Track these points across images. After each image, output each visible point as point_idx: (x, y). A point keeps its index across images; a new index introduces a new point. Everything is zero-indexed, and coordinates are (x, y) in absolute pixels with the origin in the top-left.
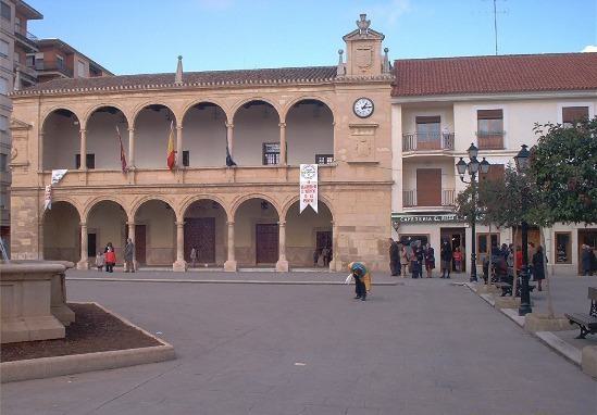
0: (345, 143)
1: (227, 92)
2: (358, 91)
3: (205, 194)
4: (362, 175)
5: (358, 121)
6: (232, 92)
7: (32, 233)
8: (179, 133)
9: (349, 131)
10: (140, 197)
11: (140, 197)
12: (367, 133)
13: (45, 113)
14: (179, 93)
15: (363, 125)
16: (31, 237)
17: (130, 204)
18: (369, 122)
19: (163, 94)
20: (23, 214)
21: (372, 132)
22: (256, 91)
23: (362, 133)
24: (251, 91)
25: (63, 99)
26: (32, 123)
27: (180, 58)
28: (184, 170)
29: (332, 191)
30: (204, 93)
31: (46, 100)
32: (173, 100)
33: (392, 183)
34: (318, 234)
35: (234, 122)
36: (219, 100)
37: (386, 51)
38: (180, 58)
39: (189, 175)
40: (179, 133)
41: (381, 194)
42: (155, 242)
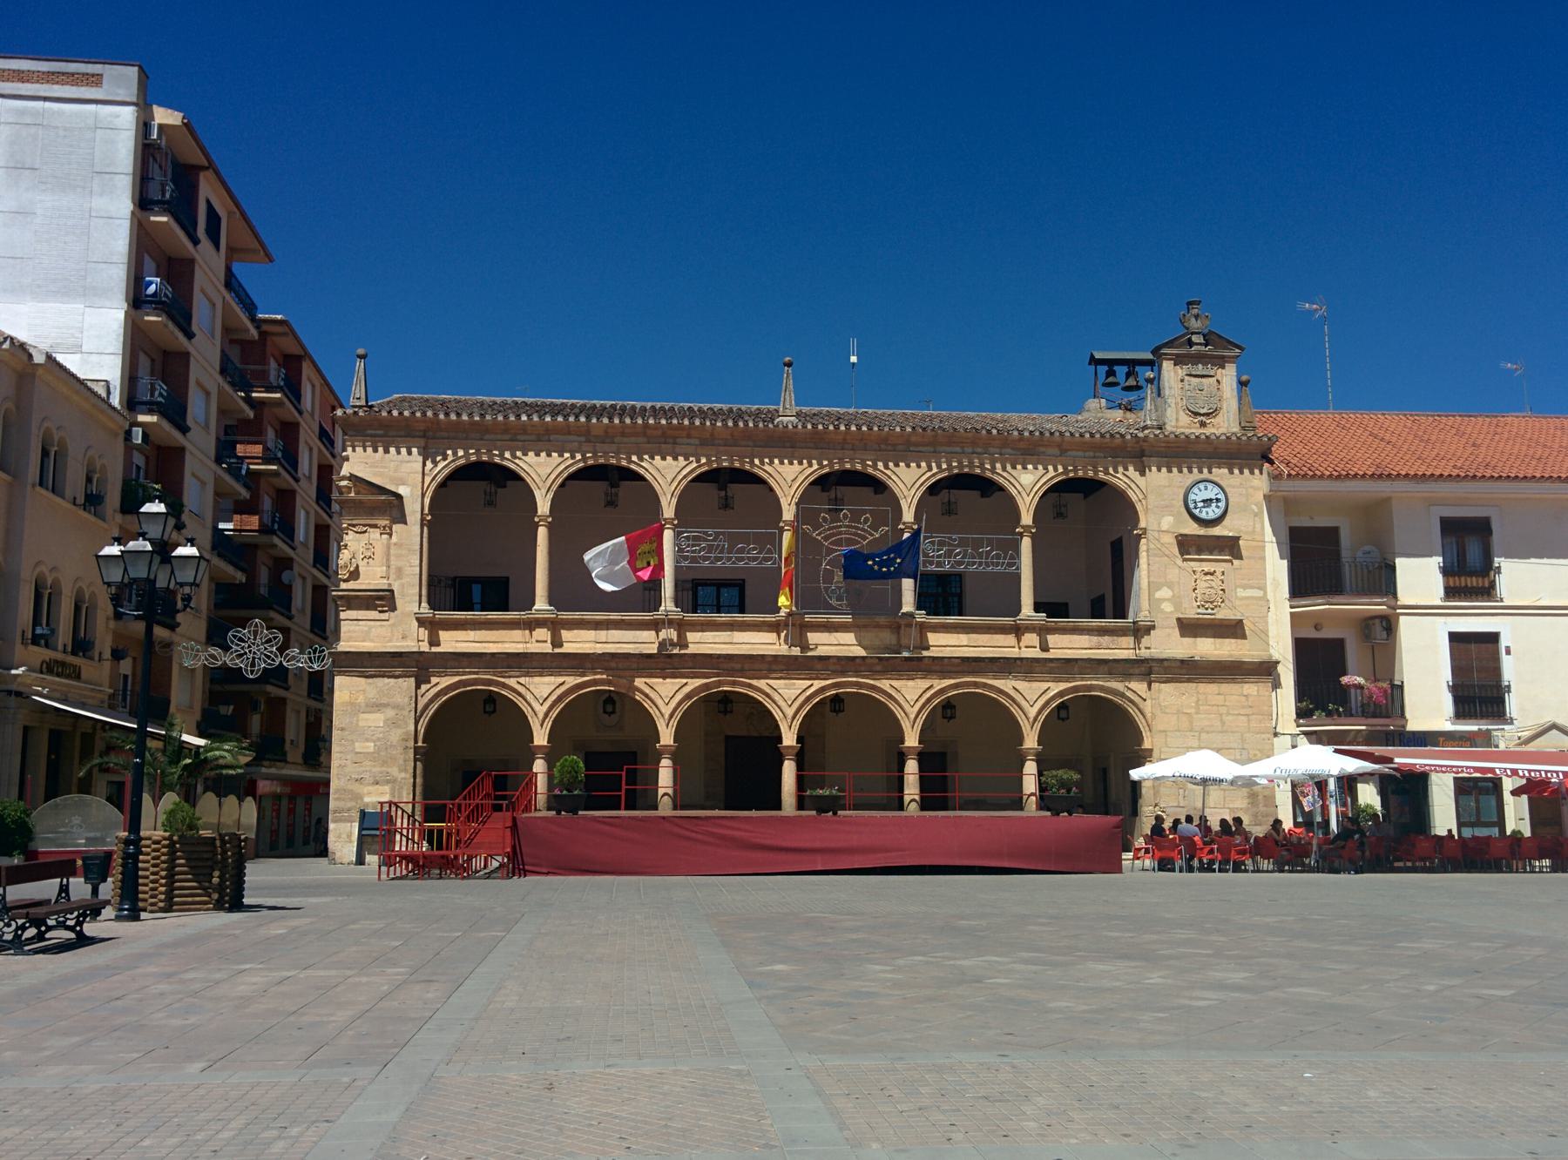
5: (1192, 529)
7: (394, 771)
15: (1208, 543)
16: (392, 781)
18: (1217, 531)
20: (376, 720)
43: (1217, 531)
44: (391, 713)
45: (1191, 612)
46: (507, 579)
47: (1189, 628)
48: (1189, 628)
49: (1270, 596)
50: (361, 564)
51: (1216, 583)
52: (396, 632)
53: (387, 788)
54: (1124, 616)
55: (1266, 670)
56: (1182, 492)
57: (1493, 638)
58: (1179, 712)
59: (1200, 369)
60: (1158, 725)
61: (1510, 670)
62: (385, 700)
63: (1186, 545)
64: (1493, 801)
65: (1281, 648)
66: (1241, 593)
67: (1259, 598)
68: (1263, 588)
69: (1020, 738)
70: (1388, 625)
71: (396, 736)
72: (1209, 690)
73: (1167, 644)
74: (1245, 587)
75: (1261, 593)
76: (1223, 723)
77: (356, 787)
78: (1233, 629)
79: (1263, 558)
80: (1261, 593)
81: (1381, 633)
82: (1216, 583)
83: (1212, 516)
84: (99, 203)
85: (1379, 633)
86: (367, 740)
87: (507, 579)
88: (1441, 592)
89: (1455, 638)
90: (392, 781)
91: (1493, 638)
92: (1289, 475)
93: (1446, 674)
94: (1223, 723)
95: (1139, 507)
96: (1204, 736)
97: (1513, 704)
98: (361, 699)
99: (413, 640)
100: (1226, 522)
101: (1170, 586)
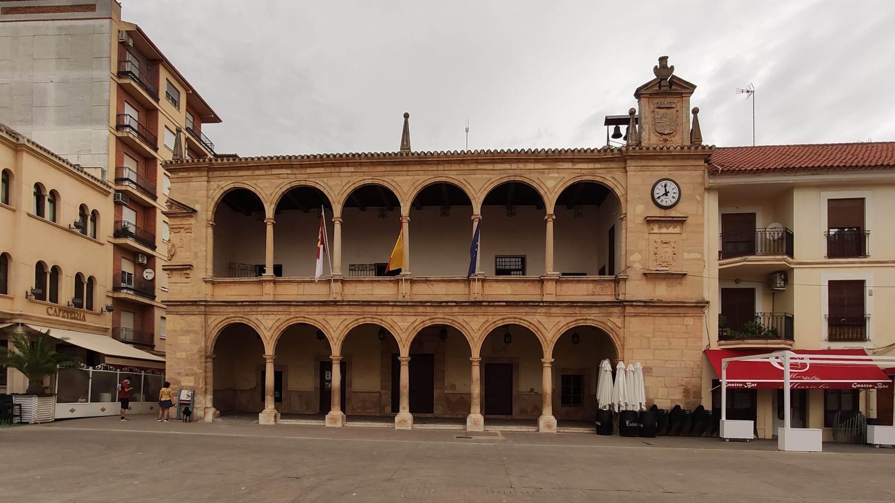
0: (637, 247)
1: (472, 167)
2: (661, 170)
3: (441, 317)
4: (662, 292)
5: (657, 212)
6: (480, 167)
7: (195, 369)
8: (338, 228)
9: (645, 228)
10: (284, 318)
11: (420, 319)
12: (671, 230)
13: (217, 195)
14: (399, 168)
15: (666, 219)
16: (195, 374)
17: (404, 329)
18: (673, 213)
19: (382, 169)
20: (185, 340)
21: (677, 230)
22: (514, 166)
23: (664, 230)
24: (507, 166)
25: (240, 173)
26: (197, 207)
27: (406, 116)
28: (275, 282)
29: (548, 315)
30: (441, 168)
31: (217, 173)
32: (397, 179)
33: (701, 305)
34: (563, 377)
35: (275, 218)
36: (461, 178)
37: (696, 111)
38: (406, 116)
39: (476, 287)
40: (338, 228)
41: (689, 321)
42: (449, 383)
44: (192, 335)
45: (653, 267)
47: (650, 276)
48: (650, 276)
49: (706, 259)
50: (178, 250)
51: (669, 250)
52: (193, 288)
53: (192, 378)
54: (728, 417)
55: (701, 305)
56: (651, 200)
57: (861, 284)
58: (542, 281)
60: (628, 345)
61: (870, 307)
62: (190, 329)
65: (712, 293)
67: (698, 259)
69: (263, 350)
70: (786, 274)
71: (195, 348)
72: (662, 323)
73: (636, 289)
74: (689, 252)
75: (699, 256)
76: (670, 344)
77: (179, 378)
79: (703, 232)
80: (699, 256)
81: (778, 280)
82: (669, 250)
83: (669, 204)
84: (96, 74)
85: (780, 283)
86: (183, 351)
88: (825, 251)
89: (832, 284)
90: (195, 374)
91: (861, 284)
92: (722, 171)
93: (825, 310)
94: (670, 344)
95: (622, 200)
96: (657, 352)
97: (871, 329)
98: (179, 328)
99: (204, 292)
100: (680, 207)
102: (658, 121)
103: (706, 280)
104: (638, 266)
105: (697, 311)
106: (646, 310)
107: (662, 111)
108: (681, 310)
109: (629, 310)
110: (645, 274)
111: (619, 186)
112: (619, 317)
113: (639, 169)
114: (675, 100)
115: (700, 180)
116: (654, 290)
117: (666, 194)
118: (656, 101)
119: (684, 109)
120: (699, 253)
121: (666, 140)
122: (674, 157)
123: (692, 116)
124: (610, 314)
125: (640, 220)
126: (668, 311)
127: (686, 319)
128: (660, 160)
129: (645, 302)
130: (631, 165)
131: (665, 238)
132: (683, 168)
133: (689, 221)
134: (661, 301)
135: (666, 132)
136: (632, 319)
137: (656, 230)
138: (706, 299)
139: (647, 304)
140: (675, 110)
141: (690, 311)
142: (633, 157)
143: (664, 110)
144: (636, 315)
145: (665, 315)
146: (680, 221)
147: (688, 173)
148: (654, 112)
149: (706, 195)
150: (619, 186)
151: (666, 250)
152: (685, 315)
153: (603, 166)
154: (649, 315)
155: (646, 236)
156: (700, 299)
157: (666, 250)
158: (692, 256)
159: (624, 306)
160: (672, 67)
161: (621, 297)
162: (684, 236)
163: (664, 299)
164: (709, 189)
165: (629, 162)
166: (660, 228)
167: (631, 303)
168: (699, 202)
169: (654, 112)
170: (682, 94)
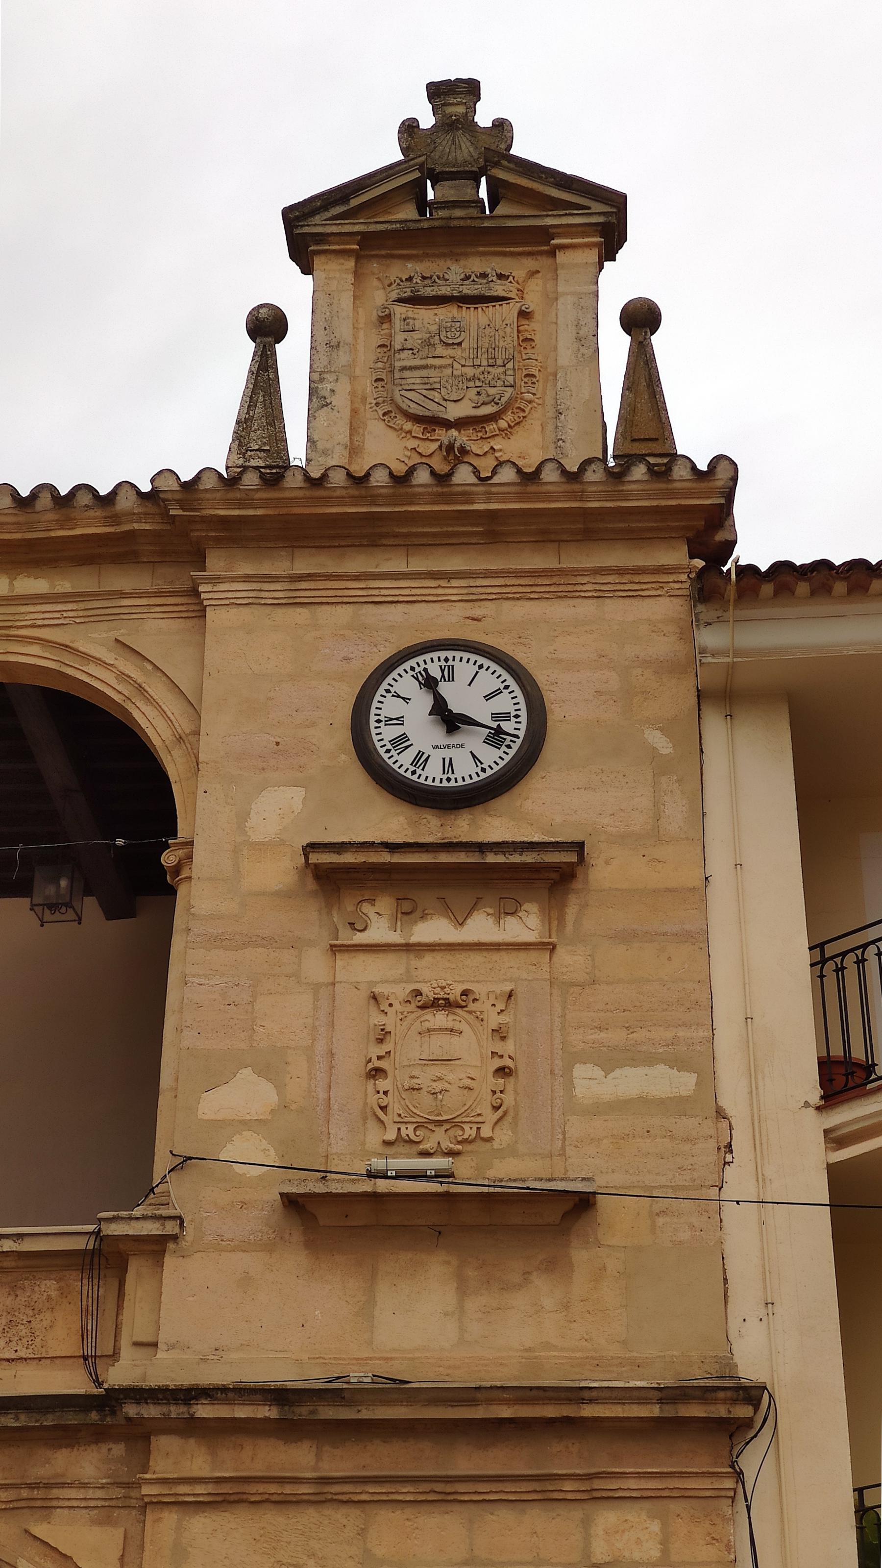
4: (424, 1324)
5: (388, 822)
9: (310, 921)
12: (481, 927)
15: (447, 857)
18: (493, 826)
21: (526, 925)
23: (434, 929)
27: (469, 685)
33: (712, 1420)
37: (641, 319)
38: (469, 685)
43: (493, 826)
45: (354, 1154)
46: (430, 86)
47: (332, 1220)
48: (332, 1220)
49: (732, 1096)
51: (468, 1047)
56: (349, 693)
59: (454, 274)
63: (336, 876)
64: (315, 366)
66: (590, 1082)
67: (677, 1106)
68: (701, 1061)
73: (228, 1312)
74: (609, 1060)
78: (548, 1219)
79: (700, 939)
87: (430, 86)
95: (174, 766)
101: (270, 1068)
102: (405, 359)
103: (740, 1229)
104: (251, 1153)
105: (696, 1459)
106: (300, 1458)
107: (427, 318)
108: (564, 1458)
109: (177, 1459)
110: (294, 1204)
111: (157, 689)
112: (105, 1515)
113: (278, 590)
114: (518, 268)
115: (665, 646)
116: (366, 1311)
117: (451, 721)
118: (398, 270)
119: (566, 309)
120: (679, 1063)
121: (456, 455)
122: (494, 530)
123: (614, 346)
124: (40, 1498)
125: (281, 871)
126: (466, 1461)
127: (607, 1518)
128: (412, 544)
129: (279, 1395)
130: (228, 574)
131: (433, 974)
132: (559, 584)
133: (605, 871)
134: (395, 1389)
135: (454, 412)
136: (200, 1525)
137: (380, 929)
138: (750, 1371)
139: (298, 1411)
140: (509, 311)
141: (634, 1464)
142: (238, 534)
143: (445, 313)
144: (229, 1496)
145: (443, 1493)
146: (550, 874)
147: (586, 608)
148: (386, 318)
149: (715, 728)
150: (157, 689)
151: (438, 1045)
152: (594, 1494)
153: (64, 586)
154: (325, 1493)
155: (315, 964)
156: (697, 1375)
157: (438, 1045)
158: (630, 1081)
159: (139, 1436)
160: (502, 127)
161: (118, 1375)
162: (571, 960)
163: (422, 1376)
164: (724, 695)
165: (216, 562)
166: (408, 913)
167: (182, 1406)
168: (661, 768)
169: (386, 318)
170: (544, 234)
